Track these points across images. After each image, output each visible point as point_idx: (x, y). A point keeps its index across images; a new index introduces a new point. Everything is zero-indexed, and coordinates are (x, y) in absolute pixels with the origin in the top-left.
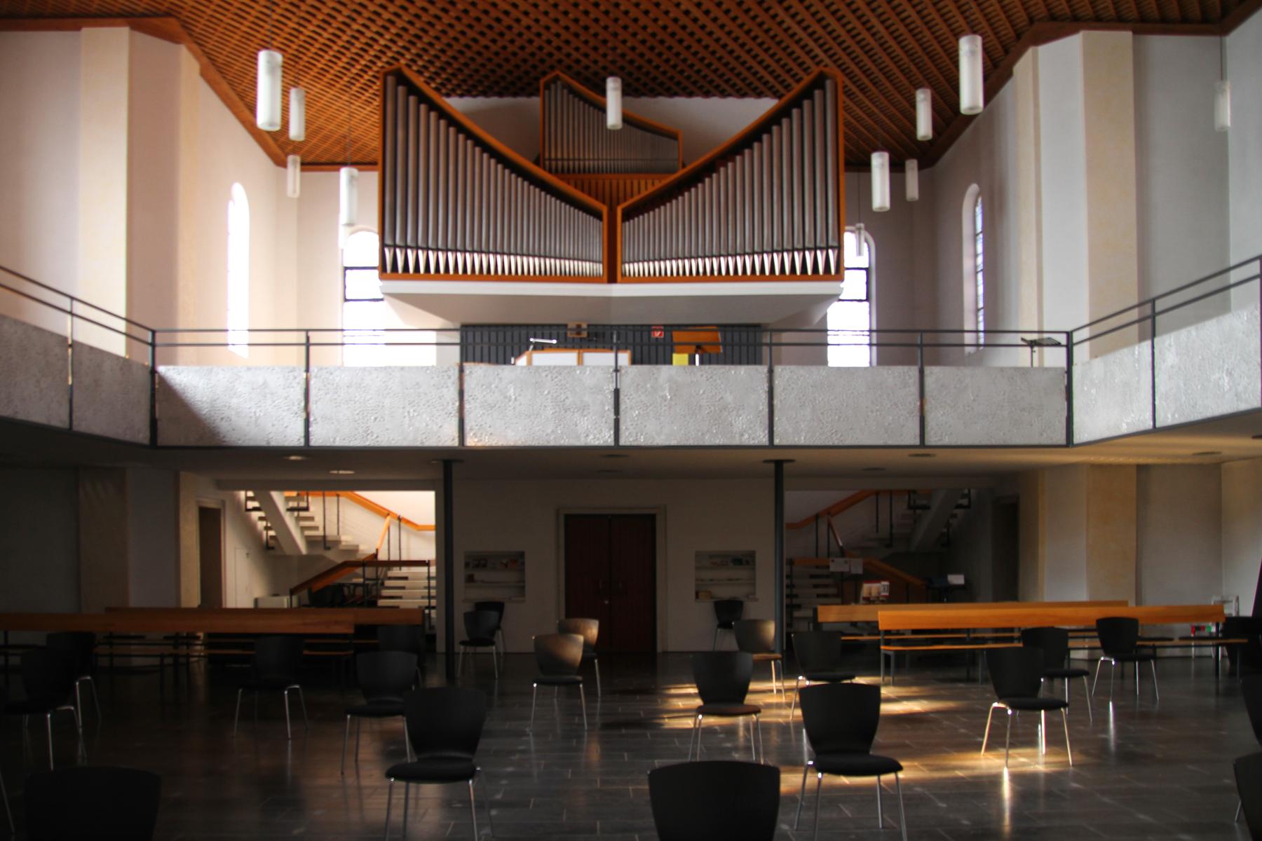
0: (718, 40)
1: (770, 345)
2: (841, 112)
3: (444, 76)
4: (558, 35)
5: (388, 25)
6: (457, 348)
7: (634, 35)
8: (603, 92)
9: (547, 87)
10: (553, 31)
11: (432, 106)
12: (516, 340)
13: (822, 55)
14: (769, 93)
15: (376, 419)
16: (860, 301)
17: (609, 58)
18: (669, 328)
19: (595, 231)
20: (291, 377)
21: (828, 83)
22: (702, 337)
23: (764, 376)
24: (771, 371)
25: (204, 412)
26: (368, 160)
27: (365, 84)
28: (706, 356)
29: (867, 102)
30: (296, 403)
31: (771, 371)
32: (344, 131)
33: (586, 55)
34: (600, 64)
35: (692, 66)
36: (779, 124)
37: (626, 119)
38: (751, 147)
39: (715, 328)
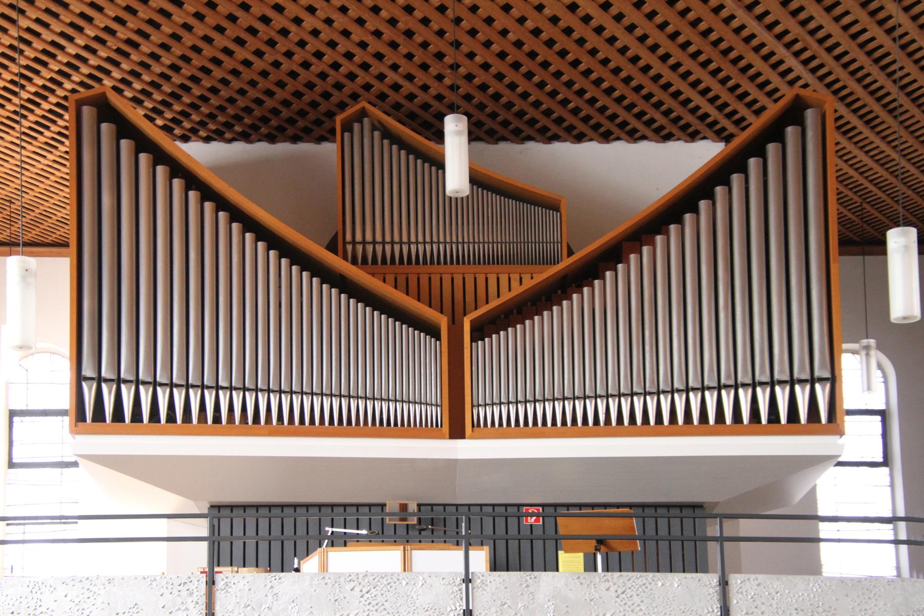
0: (623, 50)
1: (721, 539)
2: (832, 159)
3: (177, 107)
4: (363, 45)
5: (80, 22)
6: (204, 545)
7: (488, 44)
8: (439, 137)
9: (347, 127)
10: (355, 38)
11: (160, 157)
12: (301, 530)
13: (799, 69)
14: (708, 132)
17: (447, 81)
18: (551, 510)
22: (608, 526)
23: (711, 591)
24: (724, 583)
26: (50, 239)
27: (44, 117)
28: (614, 556)
29: (877, 141)
31: (724, 583)
33: (410, 77)
34: (433, 91)
35: (581, 93)
37: (475, 180)
38: (680, 221)
39: (627, 510)
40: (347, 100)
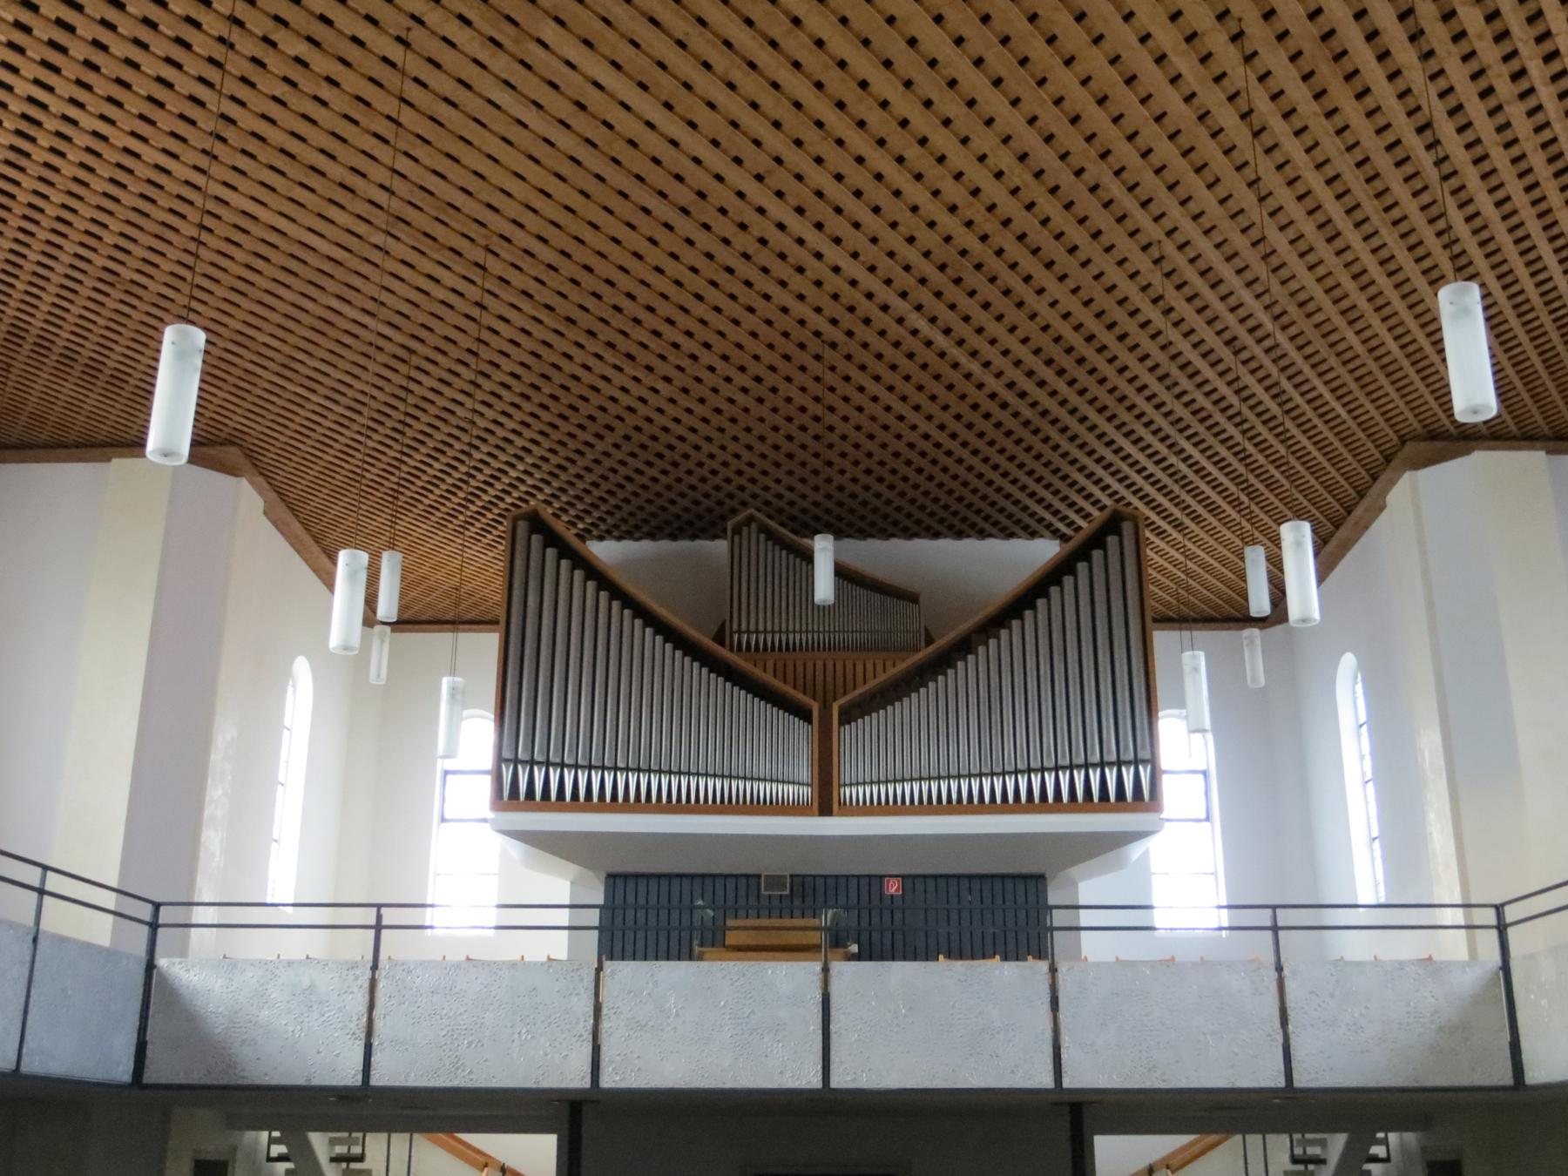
9: (737, 531)
15: (470, 1044)
16: (1198, 820)
19: (799, 739)
20: (351, 978)
21: (1127, 527)
25: (219, 1031)
26: (487, 617)
30: (355, 1017)
32: (455, 581)
36: (1059, 583)
40: (738, 506)
